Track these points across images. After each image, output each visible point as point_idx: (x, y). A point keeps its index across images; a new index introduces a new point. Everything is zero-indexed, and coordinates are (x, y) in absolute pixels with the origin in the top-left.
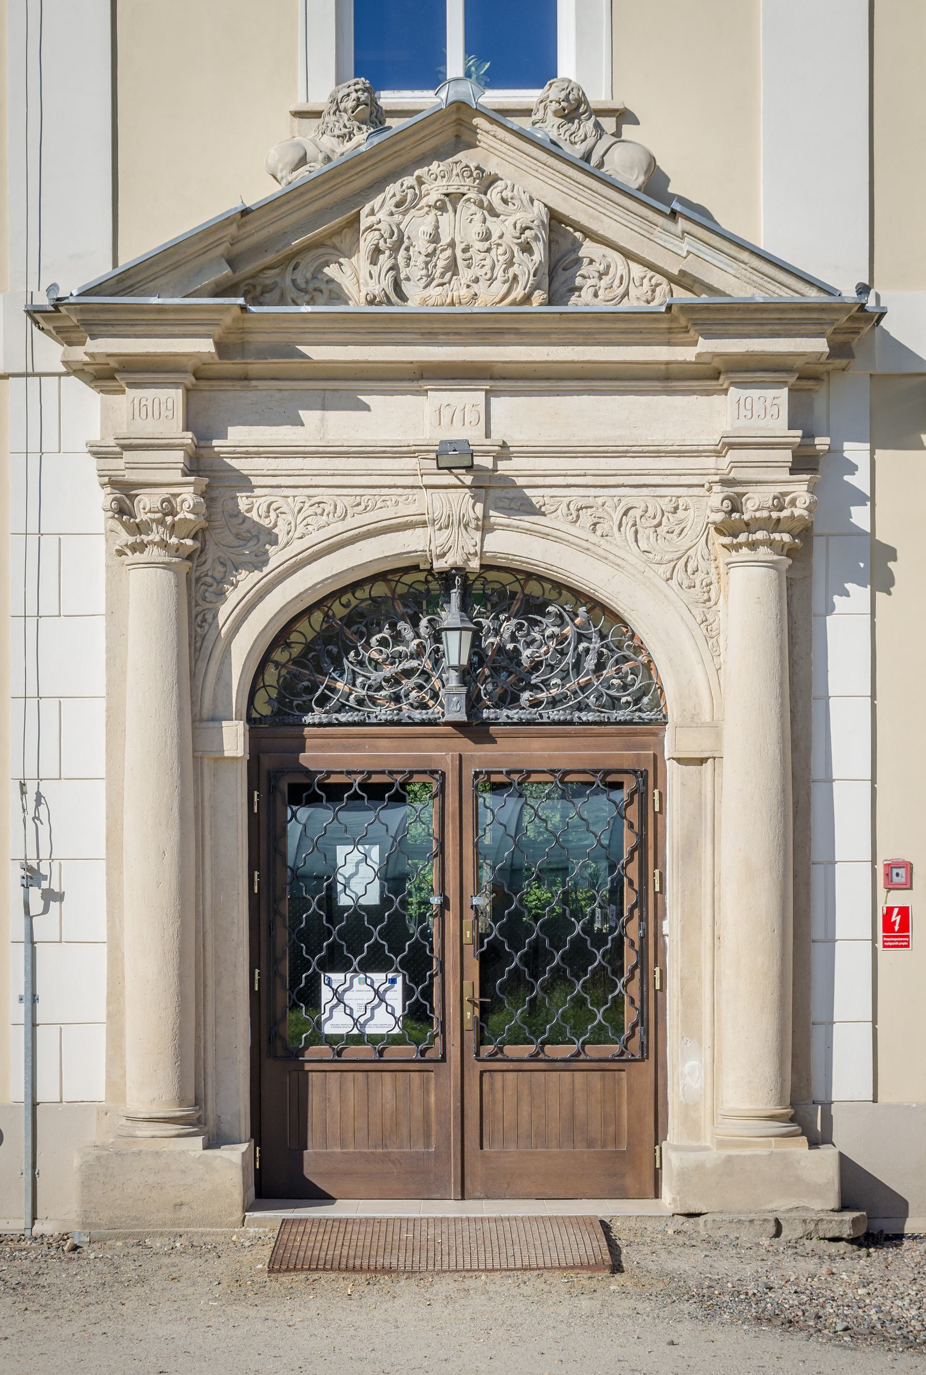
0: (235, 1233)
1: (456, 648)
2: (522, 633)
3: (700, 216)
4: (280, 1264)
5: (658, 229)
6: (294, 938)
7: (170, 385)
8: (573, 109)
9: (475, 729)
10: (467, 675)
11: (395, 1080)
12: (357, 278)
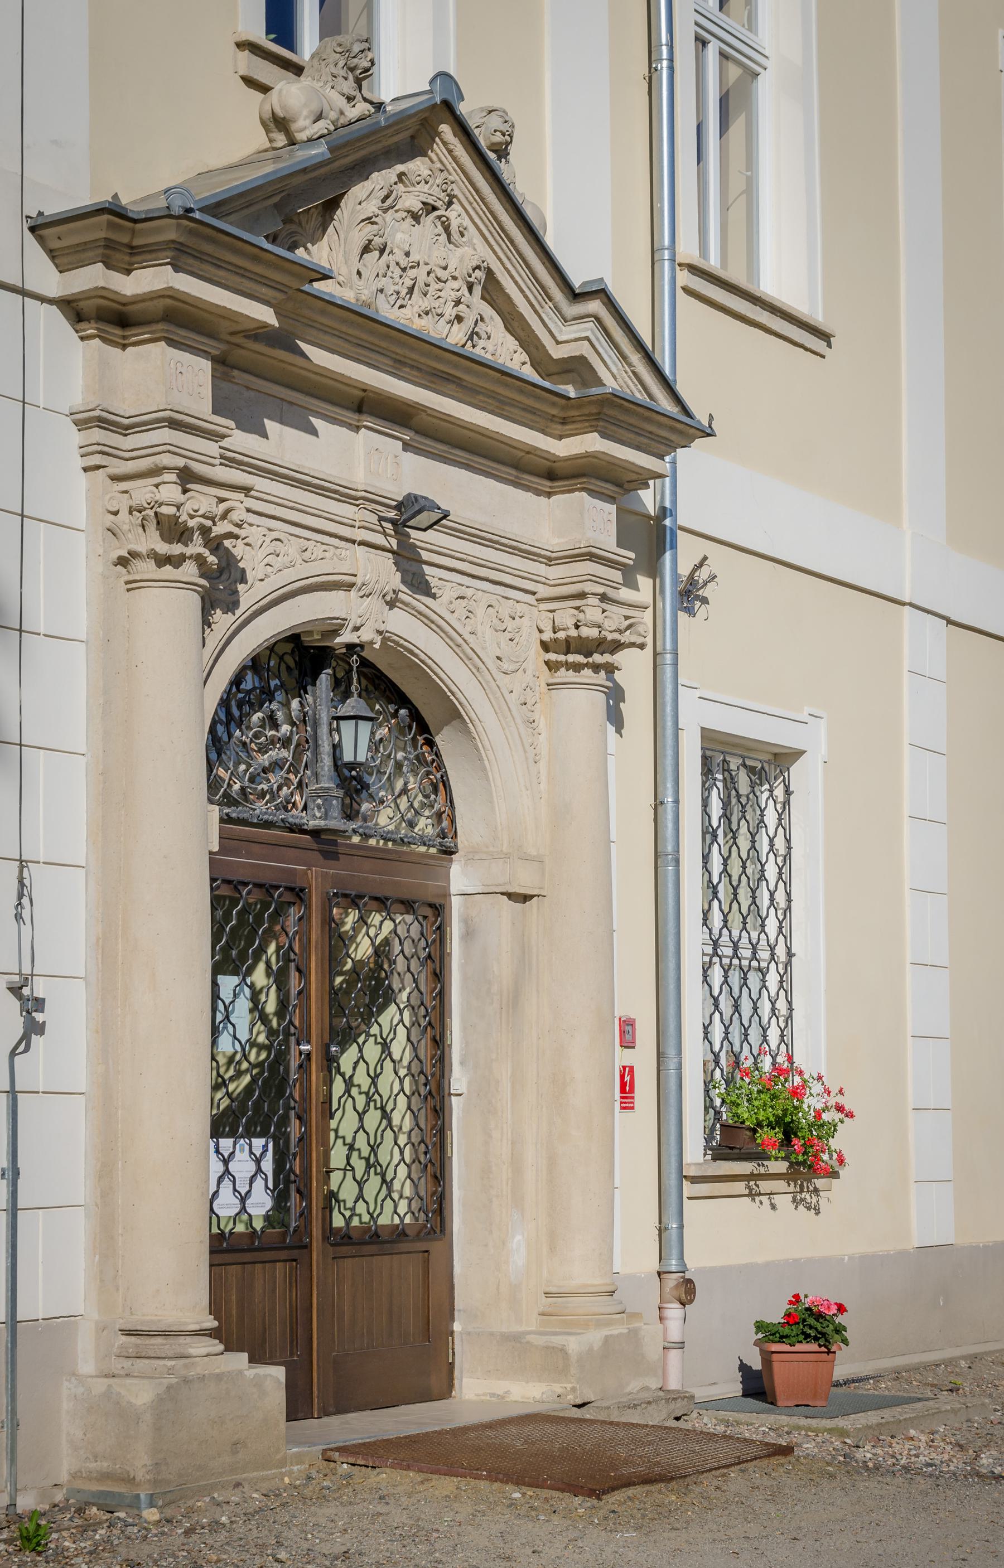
0: (283, 1475)
5: (550, 304)
7: (202, 354)
11: (264, 1268)
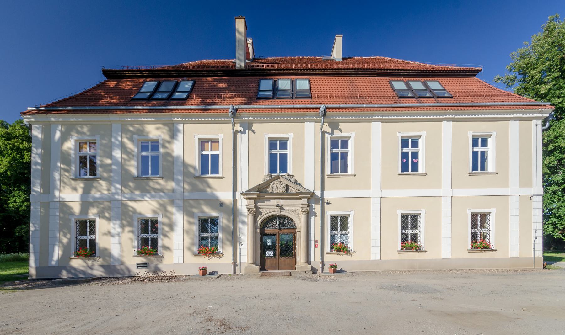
1: (278, 222)
2: (285, 222)
3: (300, 185)
4: (261, 276)
6: (264, 248)
8: (288, 175)
9: (280, 229)
10: (279, 225)
12: (270, 190)
